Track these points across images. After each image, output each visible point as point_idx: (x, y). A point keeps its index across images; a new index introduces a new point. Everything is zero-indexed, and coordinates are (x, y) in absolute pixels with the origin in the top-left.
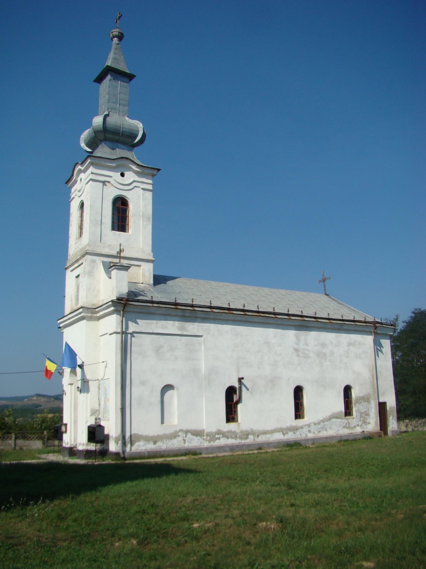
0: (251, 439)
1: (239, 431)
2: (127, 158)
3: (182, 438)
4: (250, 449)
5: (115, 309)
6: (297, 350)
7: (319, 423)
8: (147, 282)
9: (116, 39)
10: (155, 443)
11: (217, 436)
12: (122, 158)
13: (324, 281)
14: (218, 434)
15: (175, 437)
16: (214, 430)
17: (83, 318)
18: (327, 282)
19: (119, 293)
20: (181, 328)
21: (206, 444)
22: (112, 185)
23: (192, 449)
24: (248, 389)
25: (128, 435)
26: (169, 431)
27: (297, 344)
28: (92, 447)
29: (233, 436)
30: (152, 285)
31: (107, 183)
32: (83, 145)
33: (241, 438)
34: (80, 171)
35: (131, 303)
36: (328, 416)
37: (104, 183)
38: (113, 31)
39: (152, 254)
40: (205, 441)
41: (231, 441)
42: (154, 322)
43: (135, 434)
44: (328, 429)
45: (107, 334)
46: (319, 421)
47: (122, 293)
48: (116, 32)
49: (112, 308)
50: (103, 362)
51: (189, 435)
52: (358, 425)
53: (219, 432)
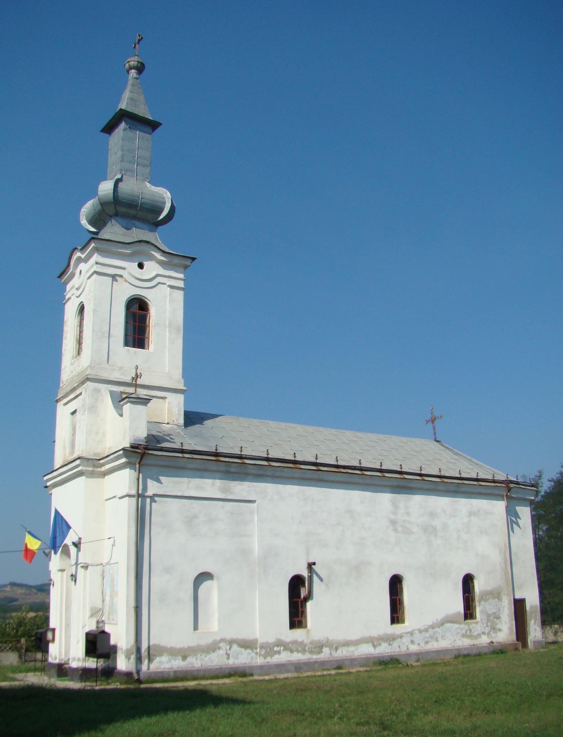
0: (326, 654)
1: (309, 642)
2: (148, 242)
3: (225, 652)
4: (325, 668)
5: (127, 460)
6: (393, 522)
7: (426, 630)
8: (175, 422)
9: (133, 71)
10: (184, 658)
11: (276, 649)
12: (140, 241)
13: (433, 420)
14: (278, 646)
15: (214, 651)
16: (271, 639)
17: (80, 474)
18: (437, 422)
19: (134, 438)
20: (225, 490)
21: (260, 661)
22: (126, 281)
23: (238, 667)
24: (321, 580)
25: (144, 646)
26: (205, 641)
27: (395, 513)
28: (92, 663)
29: (300, 649)
30: (182, 426)
31: (118, 278)
32: (84, 222)
33: (311, 652)
34: (79, 260)
35: (151, 452)
36: (439, 620)
37: (114, 277)
38: (129, 60)
39: (182, 381)
40: (258, 657)
41: (297, 657)
42: (185, 480)
43: (155, 645)
44: (440, 639)
45: (115, 497)
46: (427, 626)
47: (138, 437)
48: (133, 61)
49: (124, 460)
50: (109, 538)
51: (235, 647)
52: (484, 633)
53: (279, 643)
